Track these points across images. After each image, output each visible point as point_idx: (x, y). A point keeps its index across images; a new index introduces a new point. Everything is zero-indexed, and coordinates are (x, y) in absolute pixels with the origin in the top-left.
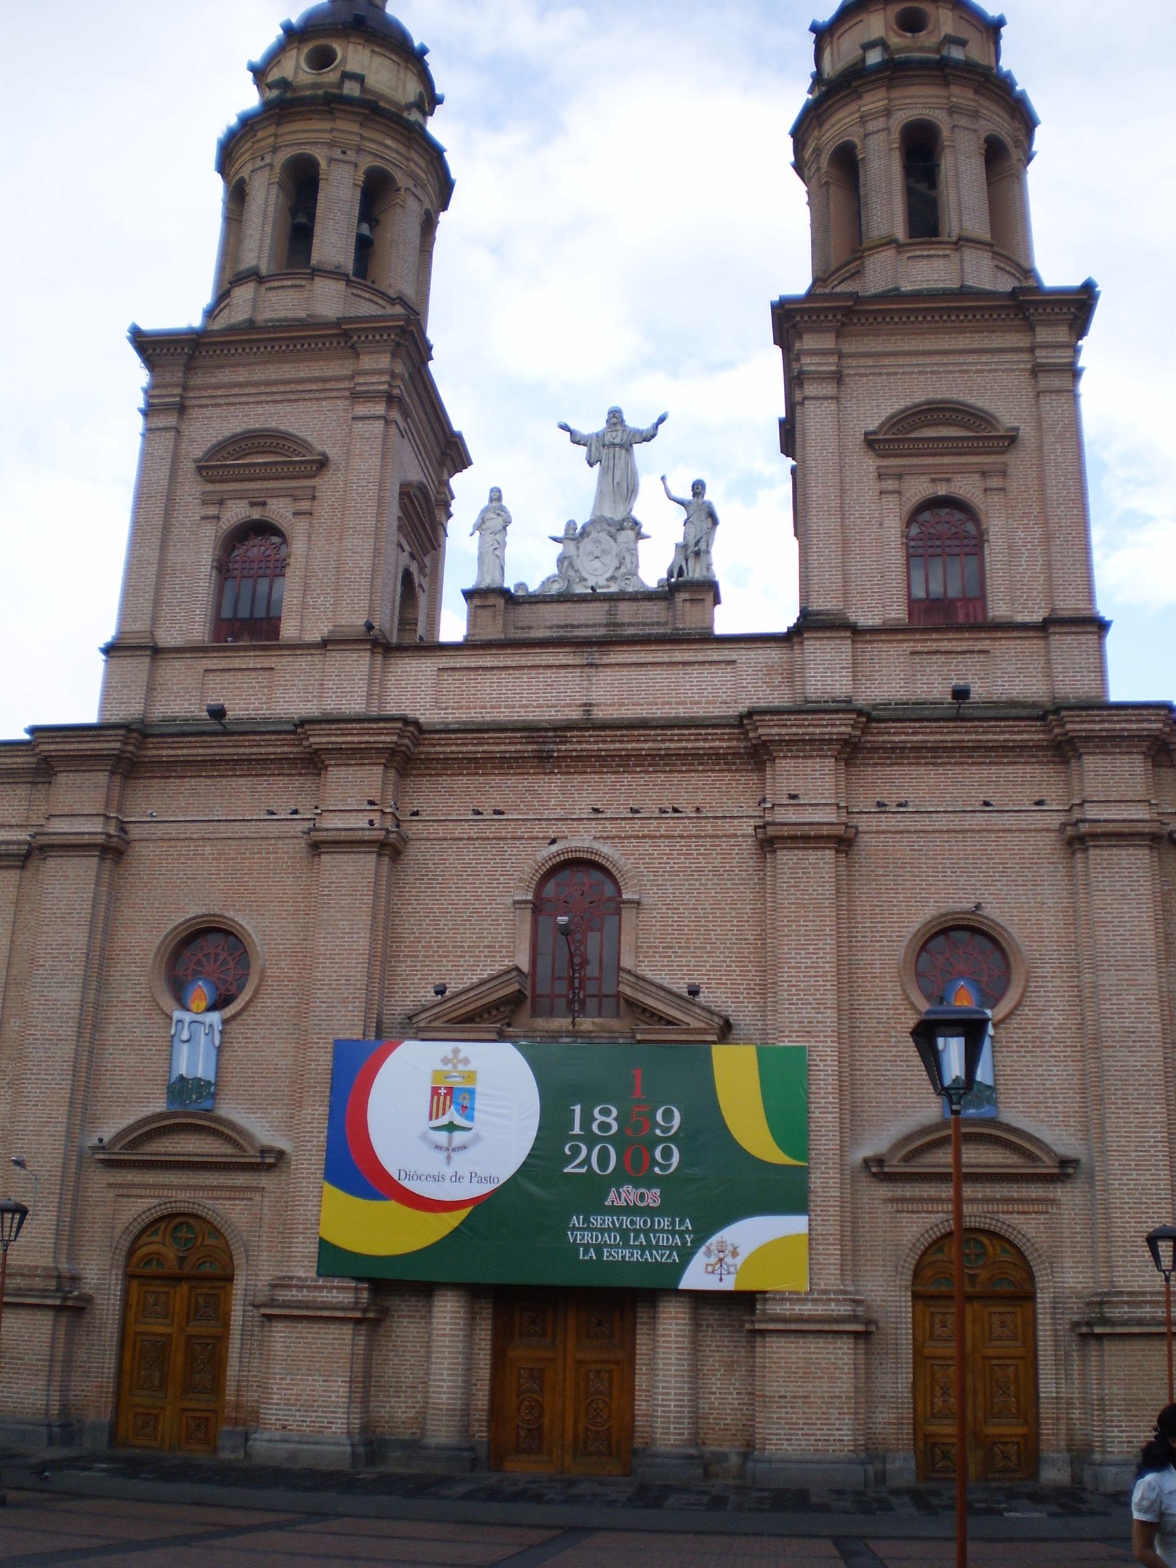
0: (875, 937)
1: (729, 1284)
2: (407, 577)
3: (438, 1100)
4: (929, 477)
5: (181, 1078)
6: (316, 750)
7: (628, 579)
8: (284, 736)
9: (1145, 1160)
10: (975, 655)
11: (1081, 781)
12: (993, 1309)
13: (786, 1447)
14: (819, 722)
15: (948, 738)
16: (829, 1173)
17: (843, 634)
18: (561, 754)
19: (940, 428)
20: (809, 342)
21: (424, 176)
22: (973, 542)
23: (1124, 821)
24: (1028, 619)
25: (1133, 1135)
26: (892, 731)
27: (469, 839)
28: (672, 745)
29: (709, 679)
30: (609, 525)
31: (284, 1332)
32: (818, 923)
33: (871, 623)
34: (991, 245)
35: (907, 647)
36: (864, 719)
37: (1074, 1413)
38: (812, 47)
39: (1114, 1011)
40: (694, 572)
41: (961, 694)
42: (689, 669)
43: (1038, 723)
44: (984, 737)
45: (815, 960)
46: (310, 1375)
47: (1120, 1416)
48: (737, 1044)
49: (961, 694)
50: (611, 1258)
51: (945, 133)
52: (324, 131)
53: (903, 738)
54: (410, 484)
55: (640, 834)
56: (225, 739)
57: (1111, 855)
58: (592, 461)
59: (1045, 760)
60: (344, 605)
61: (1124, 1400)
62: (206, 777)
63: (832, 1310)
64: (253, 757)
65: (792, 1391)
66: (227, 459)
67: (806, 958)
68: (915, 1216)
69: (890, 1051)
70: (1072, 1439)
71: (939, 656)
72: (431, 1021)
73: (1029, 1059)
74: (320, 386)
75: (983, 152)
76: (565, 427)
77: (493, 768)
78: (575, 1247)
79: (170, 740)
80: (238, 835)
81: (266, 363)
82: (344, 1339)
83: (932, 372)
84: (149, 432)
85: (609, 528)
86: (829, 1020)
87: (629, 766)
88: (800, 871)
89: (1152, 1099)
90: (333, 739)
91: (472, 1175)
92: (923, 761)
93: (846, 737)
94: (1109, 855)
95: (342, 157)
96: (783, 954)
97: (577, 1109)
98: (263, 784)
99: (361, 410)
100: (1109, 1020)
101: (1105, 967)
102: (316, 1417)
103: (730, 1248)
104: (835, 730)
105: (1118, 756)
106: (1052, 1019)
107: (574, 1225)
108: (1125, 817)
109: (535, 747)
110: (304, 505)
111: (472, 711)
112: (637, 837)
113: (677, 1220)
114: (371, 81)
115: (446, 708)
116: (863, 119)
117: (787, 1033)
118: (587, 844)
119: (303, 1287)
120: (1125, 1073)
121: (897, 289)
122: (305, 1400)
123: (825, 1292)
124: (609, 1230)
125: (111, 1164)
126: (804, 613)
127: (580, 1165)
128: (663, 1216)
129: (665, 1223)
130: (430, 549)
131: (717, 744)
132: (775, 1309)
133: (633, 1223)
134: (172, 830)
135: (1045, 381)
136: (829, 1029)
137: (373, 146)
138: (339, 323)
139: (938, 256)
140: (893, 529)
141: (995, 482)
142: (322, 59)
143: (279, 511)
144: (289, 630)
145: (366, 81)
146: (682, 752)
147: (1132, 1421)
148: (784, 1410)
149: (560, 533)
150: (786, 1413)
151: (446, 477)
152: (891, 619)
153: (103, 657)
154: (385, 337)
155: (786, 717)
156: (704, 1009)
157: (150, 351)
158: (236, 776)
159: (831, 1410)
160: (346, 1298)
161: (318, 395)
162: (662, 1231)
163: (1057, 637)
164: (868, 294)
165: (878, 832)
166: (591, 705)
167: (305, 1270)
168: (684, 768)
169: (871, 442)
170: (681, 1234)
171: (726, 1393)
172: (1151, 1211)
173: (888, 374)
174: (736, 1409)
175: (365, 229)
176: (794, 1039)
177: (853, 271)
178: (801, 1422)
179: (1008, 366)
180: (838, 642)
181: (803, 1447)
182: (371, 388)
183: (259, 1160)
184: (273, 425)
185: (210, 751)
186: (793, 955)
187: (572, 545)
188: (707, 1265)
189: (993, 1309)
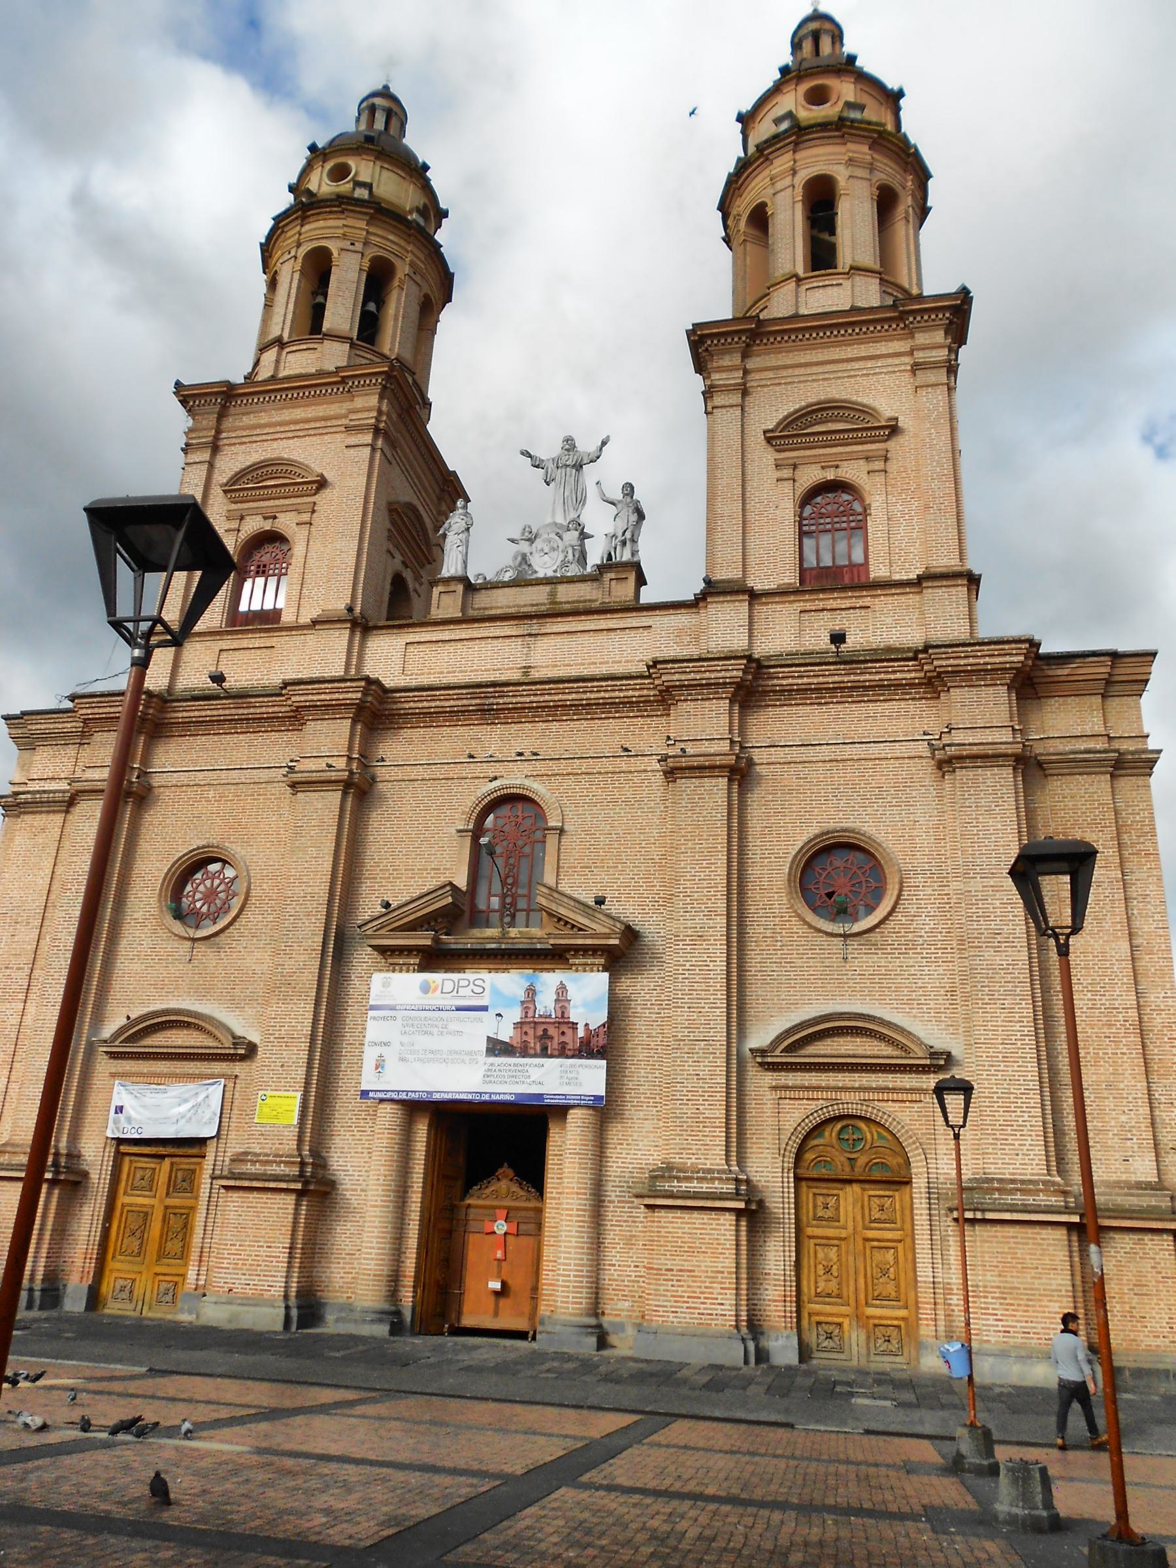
2: (398, 583)
4: (819, 465)
8: (274, 698)
12: (872, 1193)
13: (671, 1319)
14: (714, 668)
15: (830, 680)
17: (741, 597)
18: (500, 707)
21: (423, 266)
25: (1000, 1029)
26: (780, 675)
28: (593, 696)
31: (237, 1202)
32: (711, 841)
35: (799, 606)
37: (951, 1299)
39: (981, 914)
42: (613, 634)
44: (862, 678)
45: (707, 873)
46: (257, 1242)
47: (995, 1304)
53: (790, 681)
60: (1111, 1136)
61: (999, 1287)
62: (214, 734)
63: (716, 1188)
65: (678, 1265)
68: (797, 1102)
70: (951, 1326)
73: (902, 960)
74: (323, 424)
75: (875, 197)
76: (526, 454)
77: (445, 721)
79: (184, 704)
80: (235, 781)
81: (282, 409)
82: (287, 1209)
83: (824, 379)
86: (718, 926)
87: (556, 715)
88: (697, 797)
89: (1018, 995)
90: (310, 697)
92: (808, 702)
95: (351, 248)
98: (258, 739)
101: (971, 875)
102: (259, 1280)
104: (728, 674)
110: (306, 517)
115: (412, 675)
118: (518, 782)
120: (991, 972)
122: (250, 1265)
123: (710, 1171)
125: (114, 1056)
126: (708, 582)
130: (425, 562)
131: (630, 693)
134: (184, 778)
136: (719, 934)
137: (378, 240)
140: (787, 510)
143: (286, 523)
146: (601, 701)
147: (1007, 1310)
150: (672, 1286)
155: (685, 664)
156: (609, 916)
158: (237, 733)
159: (714, 1285)
161: (321, 431)
163: (930, 590)
168: (603, 716)
171: (624, 1266)
172: (1019, 1101)
174: (633, 1281)
178: (686, 1295)
179: (890, 369)
181: (688, 1320)
182: (362, 422)
183: (232, 1051)
185: (215, 713)
189: (872, 1193)
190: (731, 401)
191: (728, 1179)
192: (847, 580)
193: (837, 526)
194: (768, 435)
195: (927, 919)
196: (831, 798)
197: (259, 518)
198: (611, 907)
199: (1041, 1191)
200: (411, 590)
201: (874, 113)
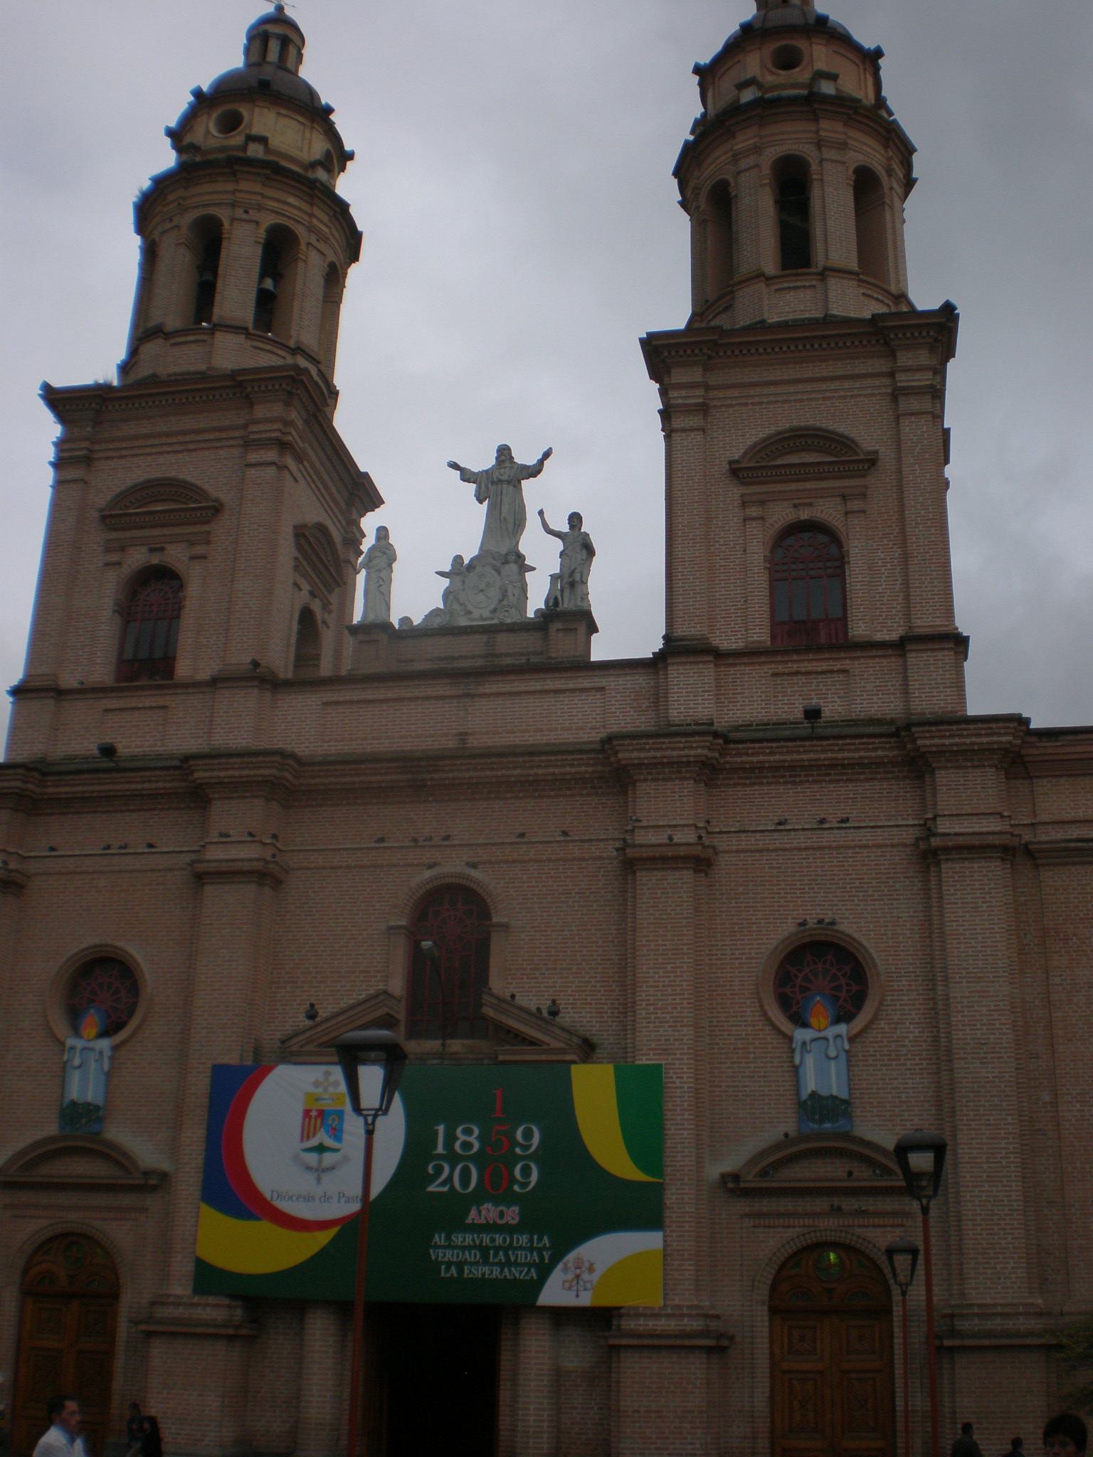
0: (735, 954)
1: (585, 1300)
2: (306, 617)
3: (309, 1123)
5: (73, 1103)
6: (201, 784)
7: (507, 611)
9: (997, 1172)
10: (835, 675)
11: (934, 795)
16: (684, 1189)
17: (706, 658)
19: (803, 454)
20: (678, 376)
22: (837, 564)
23: (974, 834)
24: (887, 638)
27: (347, 867)
28: (540, 771)
29: (579, 706)
30: (494, 559)
33: (734, 646)
34: (857, 274)
35: (768, 669)
36: (720, 741)
38: (697, 90)
40: (567, 604)
41: (812, 714)
43: (892, 740)
45: (672, 978)
48: (600, 1063)
49: (812, 714)
50: (471, 1276)
51: (814, 167)
52: (226, 192)
54: (304, 526)
55: (510, 858)
56: (119, 775)
57: (963, 867)
58: (481, 498)
59: (901, 775)
63: (685, 1326)
64: (145, 792)
66: (127, 507)
67: (664, 977)
68: (772, 1230)
69: (749, 1067)
71: (799, 677)
72: (302, 1046)
74: (217, 435)
75: (852, 183)
76: (454, 466)
78: (437, 1264)
83: (796, 401)
84: (59, 485)
85: (494, 562)
91: (341, 1195)
93: (703, 759)
94: (960, 868)
95: (245, 216)
96: (643, 973)
97: (441, 1129)
99: (254, 457)
100: (960, 1033)
103: (587, 1265)
104: (692, 753)
105: (970, 770)
106: (908, 1032)
107: (436, 1243)
108: (977, 830)
109: (409, 776)
111: (354, 743)
112: (507, 862)
113: (535, 1237)
114: (276, 142)
116: (736, 158)
117: (644, 1052)
119: (180, 1304)
121: (763, 321)
124: (469, 1248)
127: (443, 1184)
128: (522, 1233)
129: (524, 1240)
132: (629, 1324)
133: (493, 1240)
135: (906, 404)
138: (233, 375)
139: (804, 287)
140: (757, 554)
141: (855, 505)
142: (231, 123)
143: (176, 556)
144: (183, 669)
145: (270, 142)
148: (637, 1425)
149: (447, 568)
151: (354, 516)
152: (753, 642)
153: (11, 699)
154: (277, 387)
156: (563, 1029)
157: (61, 408)
158: (129, 810)
160: (219, 1315)
162: (521, 1248)
163: (914, 654)
164: (737, 326)
165: (737, 851)
166: (466, 734)
167: (181, 1288)
169: (736, 472)
170: (540, 1250)
173: (753, 404)
175: (269, 284)
176: (652, 1056)
177: (725, 305)
180: (701, 666)
184: (173, 474)
186: (651, 974)
187: (458, 579)
188: (564, 1282)
190: (691, 423)
191: (698, 1315)
192: (823, 639)
193: (812, 573)
194: (734, 466)
195: (912, 1026)
196: (807, 890)
197: (144, 549)
198: (566, 1018)
199: (1021, 1314)
200: (319, 622)
201: (852, 83)
